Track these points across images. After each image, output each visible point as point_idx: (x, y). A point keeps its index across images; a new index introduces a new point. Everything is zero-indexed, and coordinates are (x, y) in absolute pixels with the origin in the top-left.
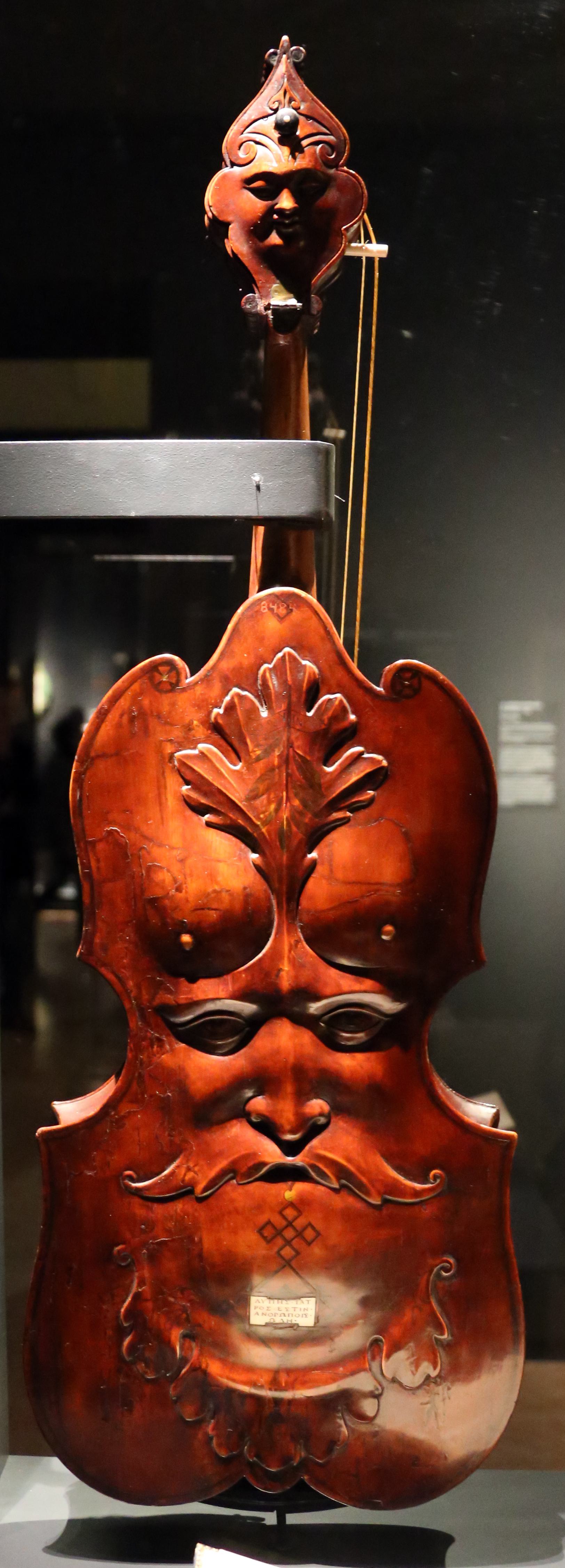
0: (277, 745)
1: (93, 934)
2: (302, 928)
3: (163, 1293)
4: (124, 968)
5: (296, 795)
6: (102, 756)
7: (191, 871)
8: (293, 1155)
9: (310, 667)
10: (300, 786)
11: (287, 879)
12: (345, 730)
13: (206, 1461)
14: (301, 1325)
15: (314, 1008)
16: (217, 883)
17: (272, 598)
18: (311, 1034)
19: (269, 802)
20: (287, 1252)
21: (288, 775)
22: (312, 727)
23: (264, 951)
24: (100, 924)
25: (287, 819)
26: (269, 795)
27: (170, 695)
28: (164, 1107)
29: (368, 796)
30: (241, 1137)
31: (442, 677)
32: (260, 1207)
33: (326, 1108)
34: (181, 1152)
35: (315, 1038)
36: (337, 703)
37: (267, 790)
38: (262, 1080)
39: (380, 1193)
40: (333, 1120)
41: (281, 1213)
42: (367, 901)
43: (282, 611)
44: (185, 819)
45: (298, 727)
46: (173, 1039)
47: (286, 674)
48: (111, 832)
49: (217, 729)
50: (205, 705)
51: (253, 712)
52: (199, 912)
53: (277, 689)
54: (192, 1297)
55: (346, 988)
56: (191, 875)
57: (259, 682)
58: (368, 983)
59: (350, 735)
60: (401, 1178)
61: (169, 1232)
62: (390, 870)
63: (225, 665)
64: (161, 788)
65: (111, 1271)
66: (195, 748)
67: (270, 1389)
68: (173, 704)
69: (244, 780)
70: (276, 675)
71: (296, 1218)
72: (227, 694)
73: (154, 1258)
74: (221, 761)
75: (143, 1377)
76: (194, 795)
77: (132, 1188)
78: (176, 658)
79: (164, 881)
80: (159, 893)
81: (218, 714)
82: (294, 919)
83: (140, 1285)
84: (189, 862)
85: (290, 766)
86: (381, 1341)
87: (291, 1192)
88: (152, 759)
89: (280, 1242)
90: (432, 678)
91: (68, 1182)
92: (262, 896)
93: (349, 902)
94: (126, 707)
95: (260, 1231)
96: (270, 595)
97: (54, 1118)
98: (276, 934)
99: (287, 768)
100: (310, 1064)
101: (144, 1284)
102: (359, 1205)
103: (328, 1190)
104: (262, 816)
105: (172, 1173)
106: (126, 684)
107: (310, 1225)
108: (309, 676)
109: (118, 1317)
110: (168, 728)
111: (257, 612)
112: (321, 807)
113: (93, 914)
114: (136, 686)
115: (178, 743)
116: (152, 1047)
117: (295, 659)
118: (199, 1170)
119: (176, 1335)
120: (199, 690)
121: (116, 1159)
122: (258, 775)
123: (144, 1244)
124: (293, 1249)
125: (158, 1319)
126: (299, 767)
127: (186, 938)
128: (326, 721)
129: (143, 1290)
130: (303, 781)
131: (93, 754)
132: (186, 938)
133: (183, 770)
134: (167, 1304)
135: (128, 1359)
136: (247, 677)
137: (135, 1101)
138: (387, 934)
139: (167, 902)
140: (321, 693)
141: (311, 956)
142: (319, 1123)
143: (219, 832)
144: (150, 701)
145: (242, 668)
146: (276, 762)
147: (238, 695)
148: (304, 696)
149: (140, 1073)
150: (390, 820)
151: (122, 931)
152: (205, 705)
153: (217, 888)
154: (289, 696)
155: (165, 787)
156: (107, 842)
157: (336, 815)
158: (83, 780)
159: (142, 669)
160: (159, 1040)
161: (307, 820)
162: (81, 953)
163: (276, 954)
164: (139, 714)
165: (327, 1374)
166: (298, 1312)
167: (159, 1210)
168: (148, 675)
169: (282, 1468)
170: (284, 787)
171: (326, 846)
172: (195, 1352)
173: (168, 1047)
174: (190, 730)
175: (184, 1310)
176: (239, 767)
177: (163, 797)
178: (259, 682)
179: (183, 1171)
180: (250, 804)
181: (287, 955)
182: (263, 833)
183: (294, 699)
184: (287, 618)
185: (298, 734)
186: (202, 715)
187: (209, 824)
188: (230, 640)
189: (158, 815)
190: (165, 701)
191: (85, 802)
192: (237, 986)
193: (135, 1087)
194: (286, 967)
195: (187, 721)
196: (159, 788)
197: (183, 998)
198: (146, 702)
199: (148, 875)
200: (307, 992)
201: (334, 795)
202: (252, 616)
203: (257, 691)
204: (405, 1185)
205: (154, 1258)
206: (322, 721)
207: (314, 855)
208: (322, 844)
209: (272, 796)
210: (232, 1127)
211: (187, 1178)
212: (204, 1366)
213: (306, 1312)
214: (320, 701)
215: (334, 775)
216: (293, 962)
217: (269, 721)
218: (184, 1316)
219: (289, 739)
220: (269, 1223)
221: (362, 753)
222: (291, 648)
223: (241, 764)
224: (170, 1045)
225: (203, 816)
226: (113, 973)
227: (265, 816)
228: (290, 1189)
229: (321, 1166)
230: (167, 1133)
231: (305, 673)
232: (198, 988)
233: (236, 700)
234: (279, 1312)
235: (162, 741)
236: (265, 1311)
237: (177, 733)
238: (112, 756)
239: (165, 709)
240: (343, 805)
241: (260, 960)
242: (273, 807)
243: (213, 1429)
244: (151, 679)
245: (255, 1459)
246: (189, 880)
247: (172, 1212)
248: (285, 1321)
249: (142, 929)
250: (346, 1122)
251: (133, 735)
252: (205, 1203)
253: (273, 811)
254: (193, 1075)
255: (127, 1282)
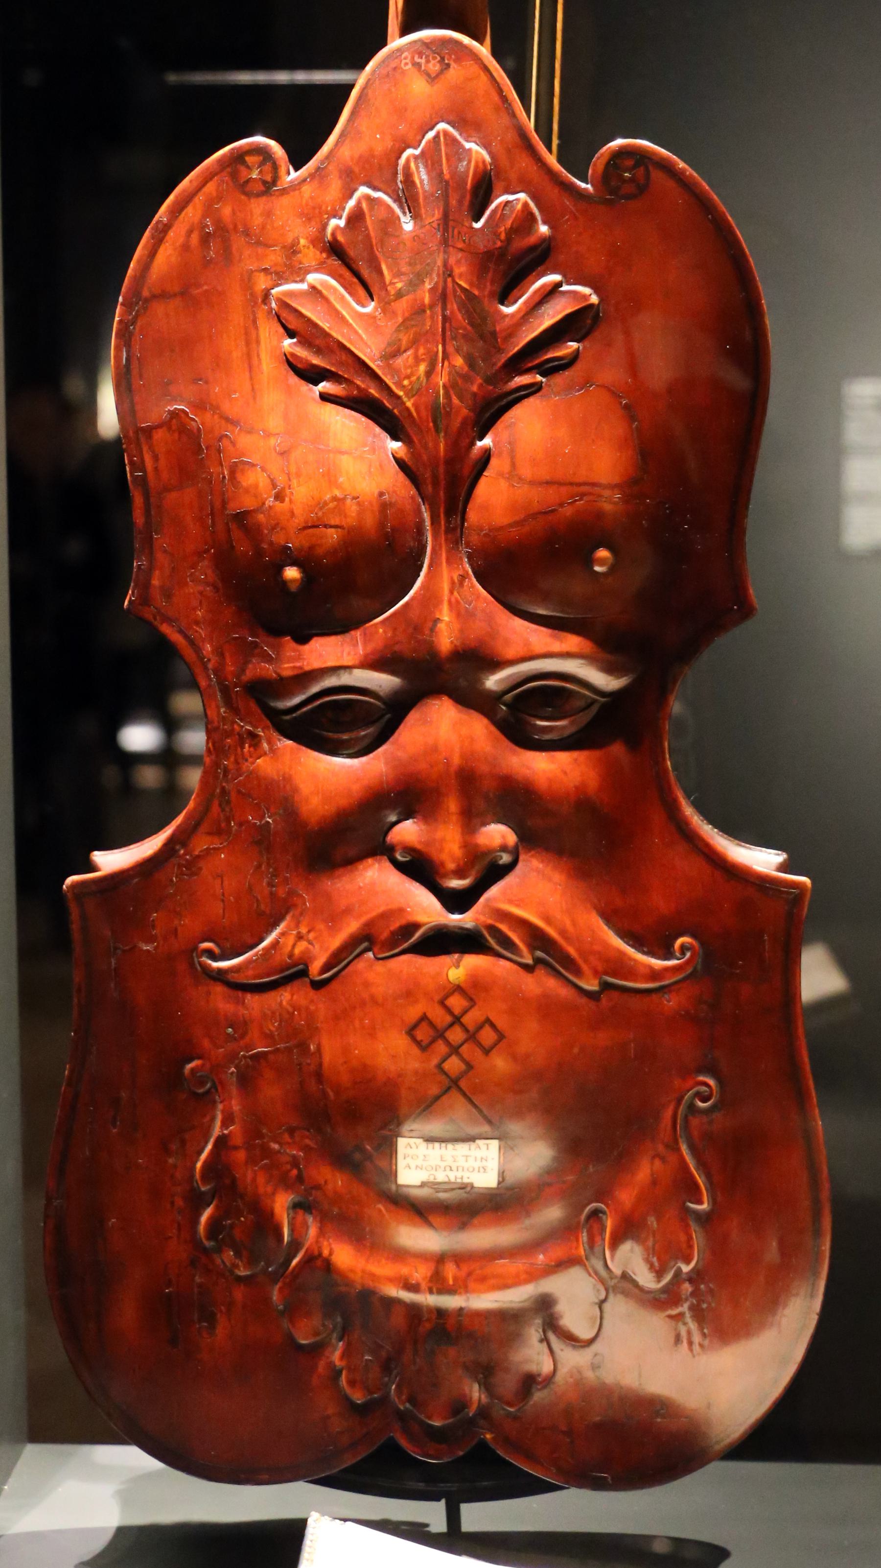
0: (429, 273)
1: (151, 569)
2: (470, 557)
3: (261, 1136)
4: (197, 623)
5: (457, 351)
6: (162, 296)
7: (298, 468)
8: (462, 913)
9: (477, 152)
10: (464, 336)
11: (446, 478)
12: (533, 248)
13: (330, 1411)
14: (476, 1185)
15: (493, 681)
16: (339, 486)
17: (418, 46)
18: (485, 721)
19: (417, 360)
20: (454, 1065)
21: (445, 319)
22: (481, 245)
23: (412, 592)
24: (160, 556)
25: (444, 386)
26: (417, 350)
27: (263, 199)
28: (262, 840)
29: (569, 350)
30: (379, 885)
31: (682, 165)
32: (409, 995)
33: (512, 838)
34: (287, 912)
35: (493, 729)
36: (519, 207)
37: (414, 343)
38: (409, 795)
39: (596, 973)
40: (522, 857)
41: (442, 1003)
42: (568, 511)
43: (434, 67)
44: (289, 391)
45: (460, 245)
46: (275, 735)
47: (441, 165)
48: (175, 414)
49: (335, 249)
50: (317, 215)
51: (390, 223)
52: (311, 531)
53: (427, 187)
54: (307, 1141)
55: (539, 648)
56: (298, 475)
57: (400, 177)
58: (572, 642)
59: (541, 256)
60: (631, 951)
61: (269, 1038)
62: (604, 463)
63: (347, 153)
64: (250, 341)
65: (182, 1099)
66: (302, 281)
67: (431, 1292)
68: (268, 214)
69: (378, 327)
70: (426, 166)
71: (465, 1012)
72: (350, 196)
73: (247, 1081)
74: (343, 298)
75: (232, 1272)
76: (302, 353)
77: (212, 970)
78: (272, 143)
79: (256, 486)
80: (248, 503)
81: (337, 227)
82: (457, 542)
83: (225, 1124)
84: (295, 455)
85: (449, 306)
86: (604, 1213)
87: (458, 969)
88: (236, 299)
89: (441, 1048)
90: (666, 167)
91: (113, 961)
92: (408, 507)
93: (541, 513)
94: (196, 219)
95: (411, 1032)
96: (415, 42)
97: (93, 868)
98: (430, 566)
99: (444, 309)
100: (484, 768)
101: (232, 1122)
102: (564, 992)
103: (515, 967)
104: (406, 382)
105: (275, 945)
106: (195, 184)
107: (488, 1021)
108: (476, 166)
109: (192, 1176)
110: (260, 250)
111: (395, 69)
112: (496, 368)
113: (149, 541)
114: (211, 188)
115: (277, 273)
116: (243, 748)
117: (455, 141)
118: (315, 938)
119: (282, 1204)
120: (307, 190)
121: (189, 924)
122: (400, 319)
123: (232, 1057)
124: (463, 1060)
125: (253, 1178)
126: (462, 306)
127: (292, 573)
128: (503, 236)
129: (231, 1132)
130: (469, 328)
131: (146, 293)
132: (292, 573)
133: (284, 314)
134: (266, 1152)
135: (209, 1244)
136: (382, 169)
137: (218, 831)
138: (602, 562)
139: (261, 517)
140: (494, 194)
141: (485, 599)
142: (501, 862)
143: (340, 408)
144: (233, 210)
145: (373, 156)
146: (427, 300)
147: (368, 198)
148: (468, 197)
149: (223, 788)
150: (603, 386)
151: (194, 566)
152: (317, 215)
153: (338, 493)
154: (446, 196)
155: (258, 342)
156: (169, 428)
157: (520, 380)
158: (131, 334)
159: (220, 161)
160: (253, 736)
161: (475, 388)
162: (130, 601)
163: (429, 598)
164: (215, 232)
165: (517, 1266)
166: (471, 1163)
167: (252, 1000)
168: (229, 169)
169: (451, 1420)
170: (439, 338)
171: (507, 427)
172: (312, 1232)
173: (265, 745)
174: (295, 253)
175: (295, 1162)
176: (370, 308)
177: (255, 359)
178: (400, 177)
179: (291, 940)
180: (389, 366)
181: (448, 601)
182: (407, 409)
183: (454, 202)
184: (442, 77)
185: (460, 255)
186: (312, 230)
187: (325, 397)
188: (354, 113)
189: (247, 386)
190: (257, 208)
191: (135, 365)
192: (370, 648)
193: (215, 809)
194: (445, 615)
195: (290, 240)
196: (248, 343)
197: (287, 669)
198: (226, 211)
199: (233, 473)
200: (479, 658)
201: (516, 349)
202: (388, 75)
203: (396, 191)
204: (635, 960)
205: (247, 1081)
206: (497, 234)
207: (487, 441)
208: (500, 425)
209: (421, 351)
210: (365, 869)
211: (297, 951)
212: (326, 1252)
213: (484, 1163)
214: (493, 206)
215: (515, 320)
216: (454, 606)
217: (415, 238)
218: (295, 1172)
219: (445, 264)
220: (424, 1018)
221: (559, 284)
222: (449, 123)
223: (373, 304)
224: (269, 742)
225: (316, 383)
226: (181, 632)
227: (411, 383)
228: (457, 967)
229: (503, 927)
230: (265, 881)
231: (469, 162)
232: (311, 651)
233: (364, 205)
234: (443, 1164)
235: (252, 271)
236: (419, 1162)
237: (274, 257)
238: (175, 295)
239: (257, 220)
240: (530, 365)
241: (407, 604)
242: (422, 368)
243: (342, 1358)
244: (234, 175)
245: (408, 1405)
246: (294, 482)
247: (274, 1006)
248: (453, 1179)
249: (225, 561)
250: (542, 862)
251: (207, 263)
252: (323, 991)
253: (421, 375)
254: (305, 788)
255: (206, 1120)
